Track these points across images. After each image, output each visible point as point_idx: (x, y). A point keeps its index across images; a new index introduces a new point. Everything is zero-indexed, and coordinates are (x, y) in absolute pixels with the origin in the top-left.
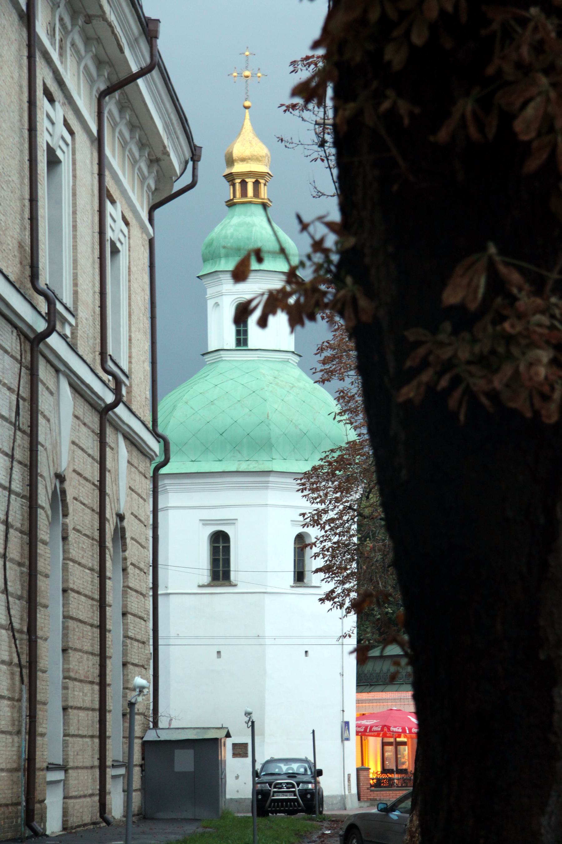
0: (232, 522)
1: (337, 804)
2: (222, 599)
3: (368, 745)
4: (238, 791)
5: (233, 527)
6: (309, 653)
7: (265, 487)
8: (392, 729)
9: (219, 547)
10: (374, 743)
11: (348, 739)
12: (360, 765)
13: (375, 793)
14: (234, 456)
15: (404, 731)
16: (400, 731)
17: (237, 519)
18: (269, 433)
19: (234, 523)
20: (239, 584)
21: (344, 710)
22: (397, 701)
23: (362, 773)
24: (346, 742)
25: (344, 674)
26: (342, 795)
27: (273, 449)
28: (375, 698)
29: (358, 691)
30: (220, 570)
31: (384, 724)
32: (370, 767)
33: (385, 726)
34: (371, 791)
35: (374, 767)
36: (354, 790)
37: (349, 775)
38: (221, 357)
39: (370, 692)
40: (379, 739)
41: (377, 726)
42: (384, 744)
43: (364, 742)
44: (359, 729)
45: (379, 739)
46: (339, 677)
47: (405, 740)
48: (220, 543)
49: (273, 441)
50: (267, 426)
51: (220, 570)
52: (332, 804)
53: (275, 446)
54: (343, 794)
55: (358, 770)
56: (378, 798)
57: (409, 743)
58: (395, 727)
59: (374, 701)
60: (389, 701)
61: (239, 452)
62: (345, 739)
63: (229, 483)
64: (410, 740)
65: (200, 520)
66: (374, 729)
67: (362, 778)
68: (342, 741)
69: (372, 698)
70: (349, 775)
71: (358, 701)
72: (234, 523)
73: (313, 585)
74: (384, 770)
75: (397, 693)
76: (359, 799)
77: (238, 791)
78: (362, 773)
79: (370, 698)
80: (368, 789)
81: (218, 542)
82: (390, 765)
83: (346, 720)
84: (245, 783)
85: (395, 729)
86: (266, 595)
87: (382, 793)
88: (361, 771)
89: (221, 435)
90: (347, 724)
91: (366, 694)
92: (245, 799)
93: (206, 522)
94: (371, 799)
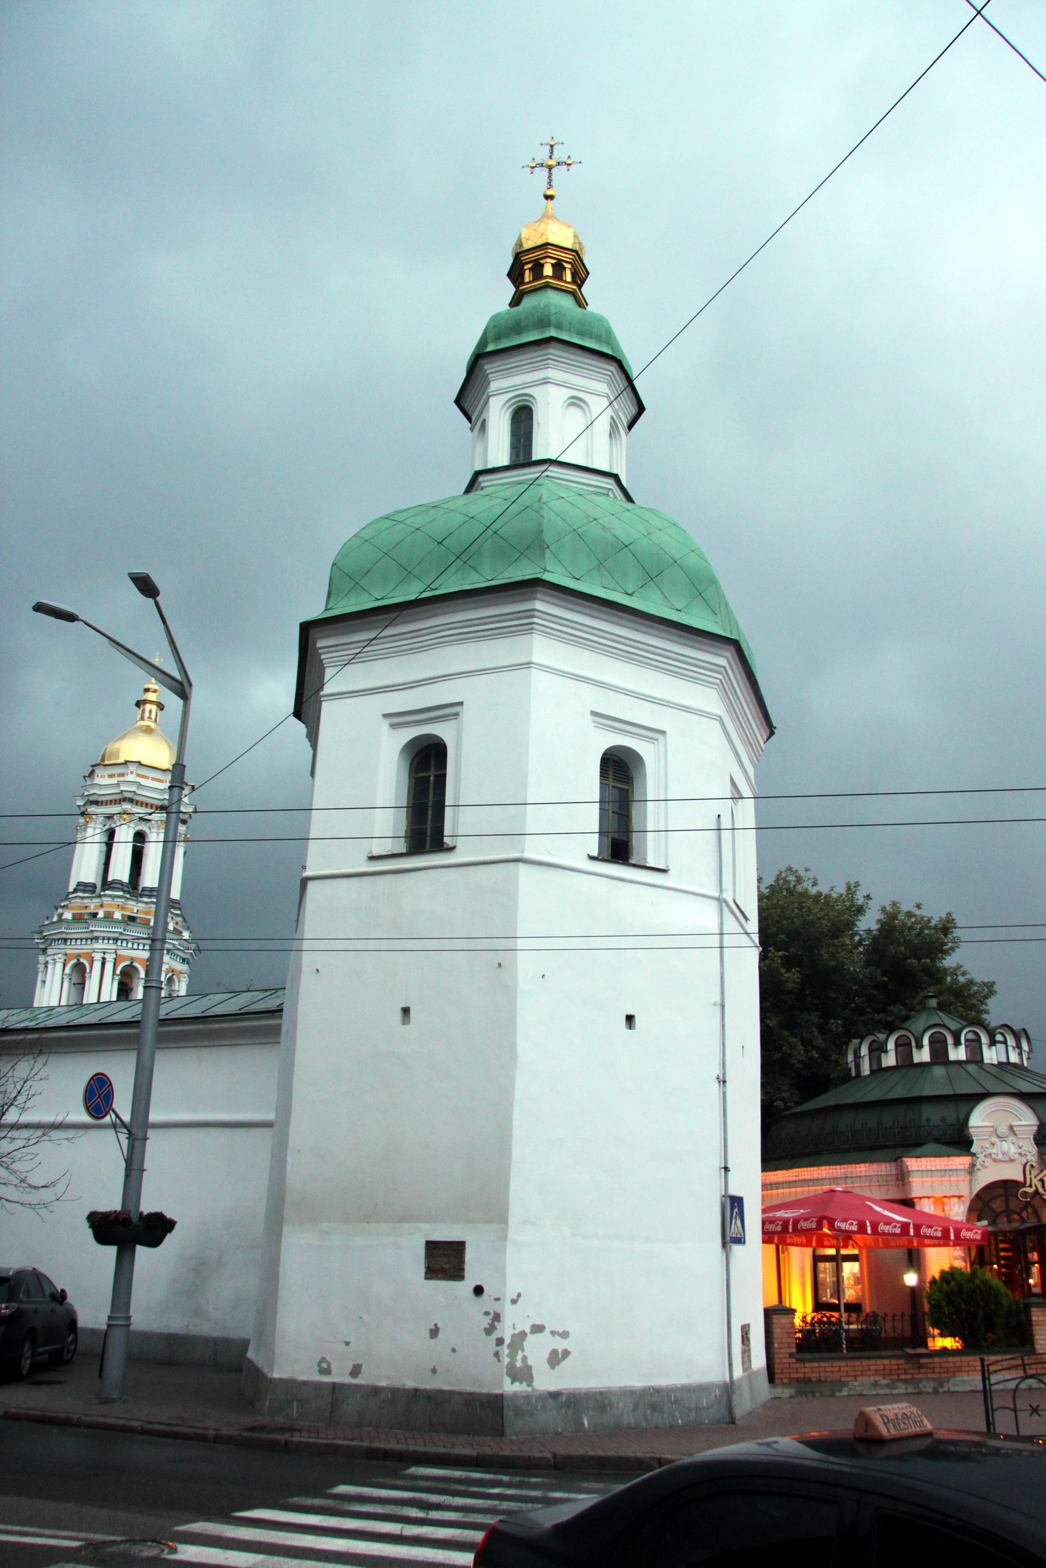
0: (450, 711)
1: (709, 1408)
2: (428, 890)
3: (789, 1260)
4: (434, 1371)
5: (452, 724)
6: (413, 1013)
7: (525, 625)
8: (837, 1224)
9: (429, 777)
10: (799, 1257)
11: (740, 1240)
12: (774, 1301)
13: (807, 1365)
14: (463, 579)
15: (862, 1228)
16: (855, 1228)
17: (461, 704)
18: (540, 523)
19: (457, 714)
20: (460, 843)
21: (729, 1166)
22: (839, 1181)
23: (779, 1320)
24: (736, 1248)
25: (727, 1079)
26: (725, 1384)
27: (547, 553)
28: (800, 1178)
29: (764, 1169)
30: (426, 826)
31: (820, 1214)
32: (794, 1307)
33: (824, 1218)
34: (799, 1361)
35: (801, 1303)
36: (759, 1360)
37: (745, 1330)
38: (533, 617)
39: (791, 1168)
40: (808, 1251)
41: (806, 1220)
42: (817, 1259)
43: (781, 1256)
44: (770, 1227)
45: (808, 1251)
46: (715, 1085)
47: (856, 1252)
48: (427, 761)
49: (548, 537)
50: (537, 512)
51: (426, 826)
52: (697, 1408)
53: (552, 548)
54: (728, 1379)
55: (769, 1313)
56: (814, 1376)
57: (864, 1258)
58: (845, 1220)
59: (799, 1184)
60: (825, 1182)
61: (475, 570)
62: (731, 1239)
63: (448, 626)
64: (864, 1251)
65: (385, 716)
66: (803, 1225)
67: (777, 1331)
68: (724, 1244)
69: (794, 1179)
70: (745, 1330)
71: (765, 1186)
72: (457, 714)
73: (651, 863)
74: (819, 1306)
75: (838, 1167)
76: (771, 1379)
77: (434, 1371)
78: (779, 1320)
79: (791, 1179)
80: (791, 1355)
81: (426, 769)
82: (828, 1297)
83: (733, 1191)
84: (454, 1350)
85: (843, 1226)
86: (521, 865)
87: (823, 1364)
88: (776, 1314)
89: (440, 543)
90: (736, 1202)
91: (784, 1171)
92: (451, 1393)
93: (397, 719)
94: (797, 1380)
